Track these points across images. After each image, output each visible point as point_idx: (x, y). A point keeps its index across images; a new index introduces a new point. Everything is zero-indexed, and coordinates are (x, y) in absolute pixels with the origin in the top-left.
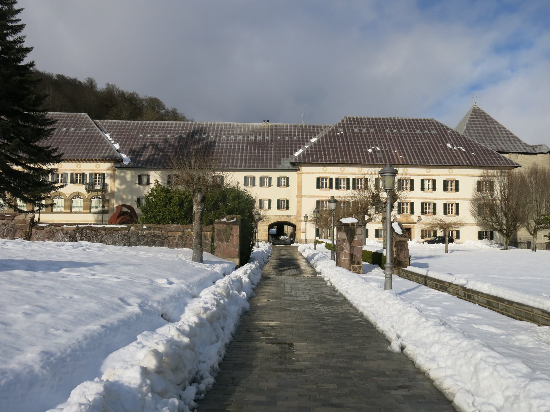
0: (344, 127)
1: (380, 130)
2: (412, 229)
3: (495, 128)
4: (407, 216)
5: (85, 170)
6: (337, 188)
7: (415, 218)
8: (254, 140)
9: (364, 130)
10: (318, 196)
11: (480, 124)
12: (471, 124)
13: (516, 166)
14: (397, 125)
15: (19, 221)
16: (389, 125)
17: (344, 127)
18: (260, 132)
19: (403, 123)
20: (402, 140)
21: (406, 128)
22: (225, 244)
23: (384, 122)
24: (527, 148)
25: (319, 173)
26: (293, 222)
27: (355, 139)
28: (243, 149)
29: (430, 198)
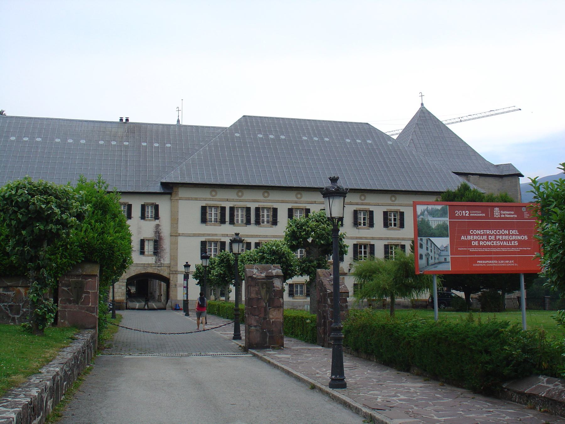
6: (258, 222)
10: (203, 235)
22: (73, 308)
26: (165, 274)
29: (366, 238)
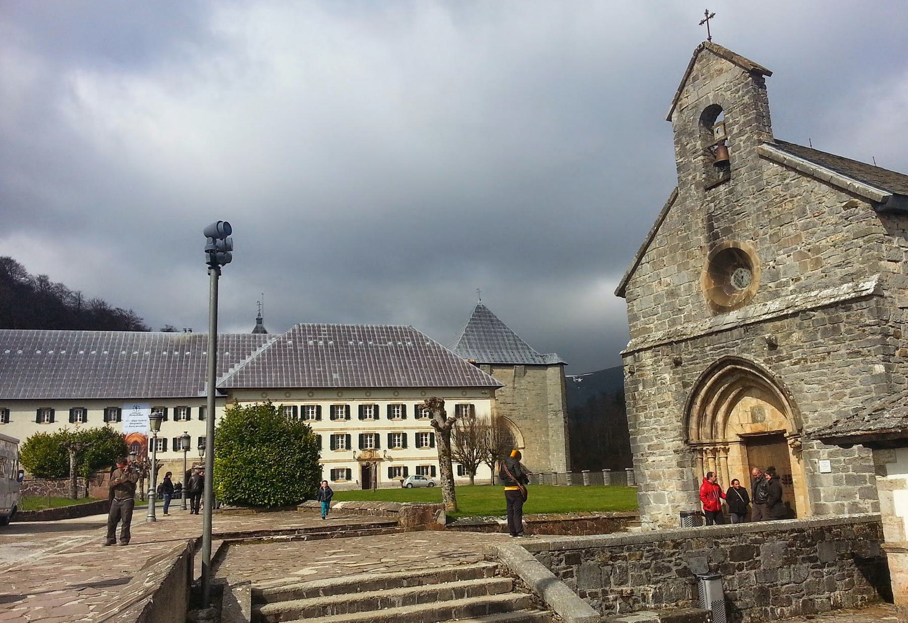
0: (294, 338)
1: (341, 343)
3: (501, 332)
4: (370, 451)
8: (168, 356)
9: (321, 343)
11: (483, 328)
12: (472, 328)
13: (498, 385)
16: (354, 335)
17: (294, 338)
18: (177, 346)
19: (373, 332)
20: (368, 355)
21: (375, 339)
23: (349, 331)
24: (536, 358)
27: (307, 354)
28: (150, 370)
29: (399, 428)
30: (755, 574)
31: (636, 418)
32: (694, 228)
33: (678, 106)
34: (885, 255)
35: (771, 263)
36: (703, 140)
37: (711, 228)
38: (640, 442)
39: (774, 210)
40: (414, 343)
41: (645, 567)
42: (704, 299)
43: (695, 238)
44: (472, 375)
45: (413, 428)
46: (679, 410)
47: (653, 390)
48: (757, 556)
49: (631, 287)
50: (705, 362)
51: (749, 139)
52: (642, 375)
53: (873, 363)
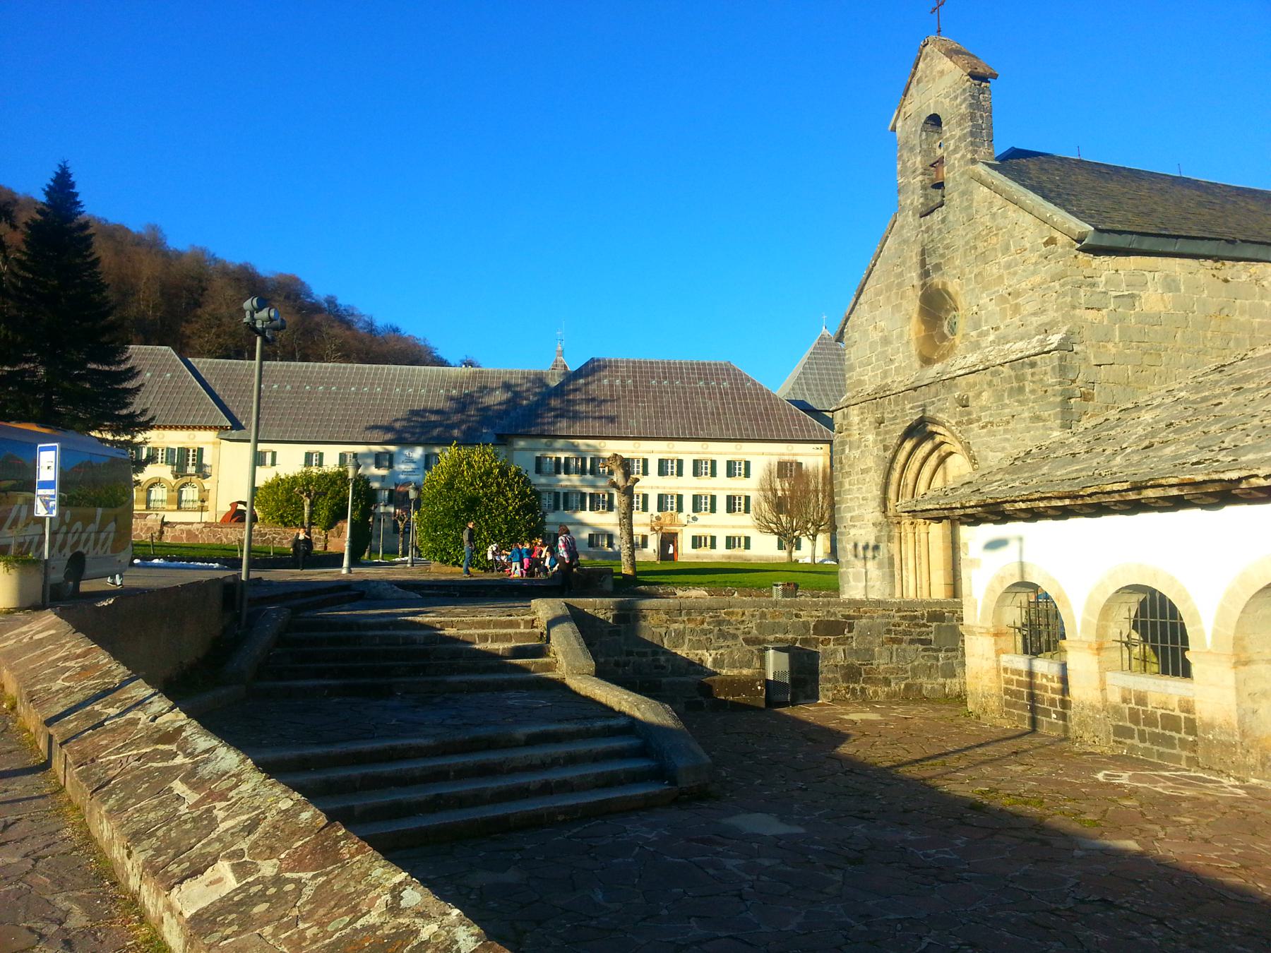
2: (679, 536)
5: (170, 442)
7: (682, 517)
9: (618, 382)
14: (670, 373)
15: (151, 520)
18: (455, 383)
25: (661, 452)
29: (707, 489)
30: (844, 650)
31: (841, 484)
32: (908, 264)
33: (902, 114)
34: (1083, 301)
35: (975, 308)
36: (923, 156)
37: (923, 263)
38: (844, 512)
39: (980, 245)
40: (731, 384)
41: (704, 632)
42: (913, 348)
43: (909, 275)
44: (800, 425)
45: (723, 489)
46: (879, 477)
47: (857, 453)
48: (849, 632)
49: (850, 331)
50: (904, 422)
51: (963, 156)
52: (849, 435)
53: (1051, 429)
